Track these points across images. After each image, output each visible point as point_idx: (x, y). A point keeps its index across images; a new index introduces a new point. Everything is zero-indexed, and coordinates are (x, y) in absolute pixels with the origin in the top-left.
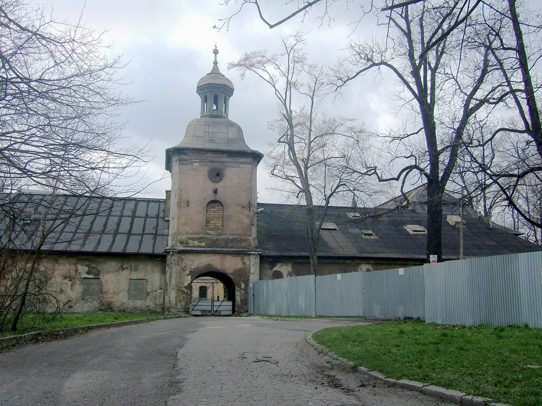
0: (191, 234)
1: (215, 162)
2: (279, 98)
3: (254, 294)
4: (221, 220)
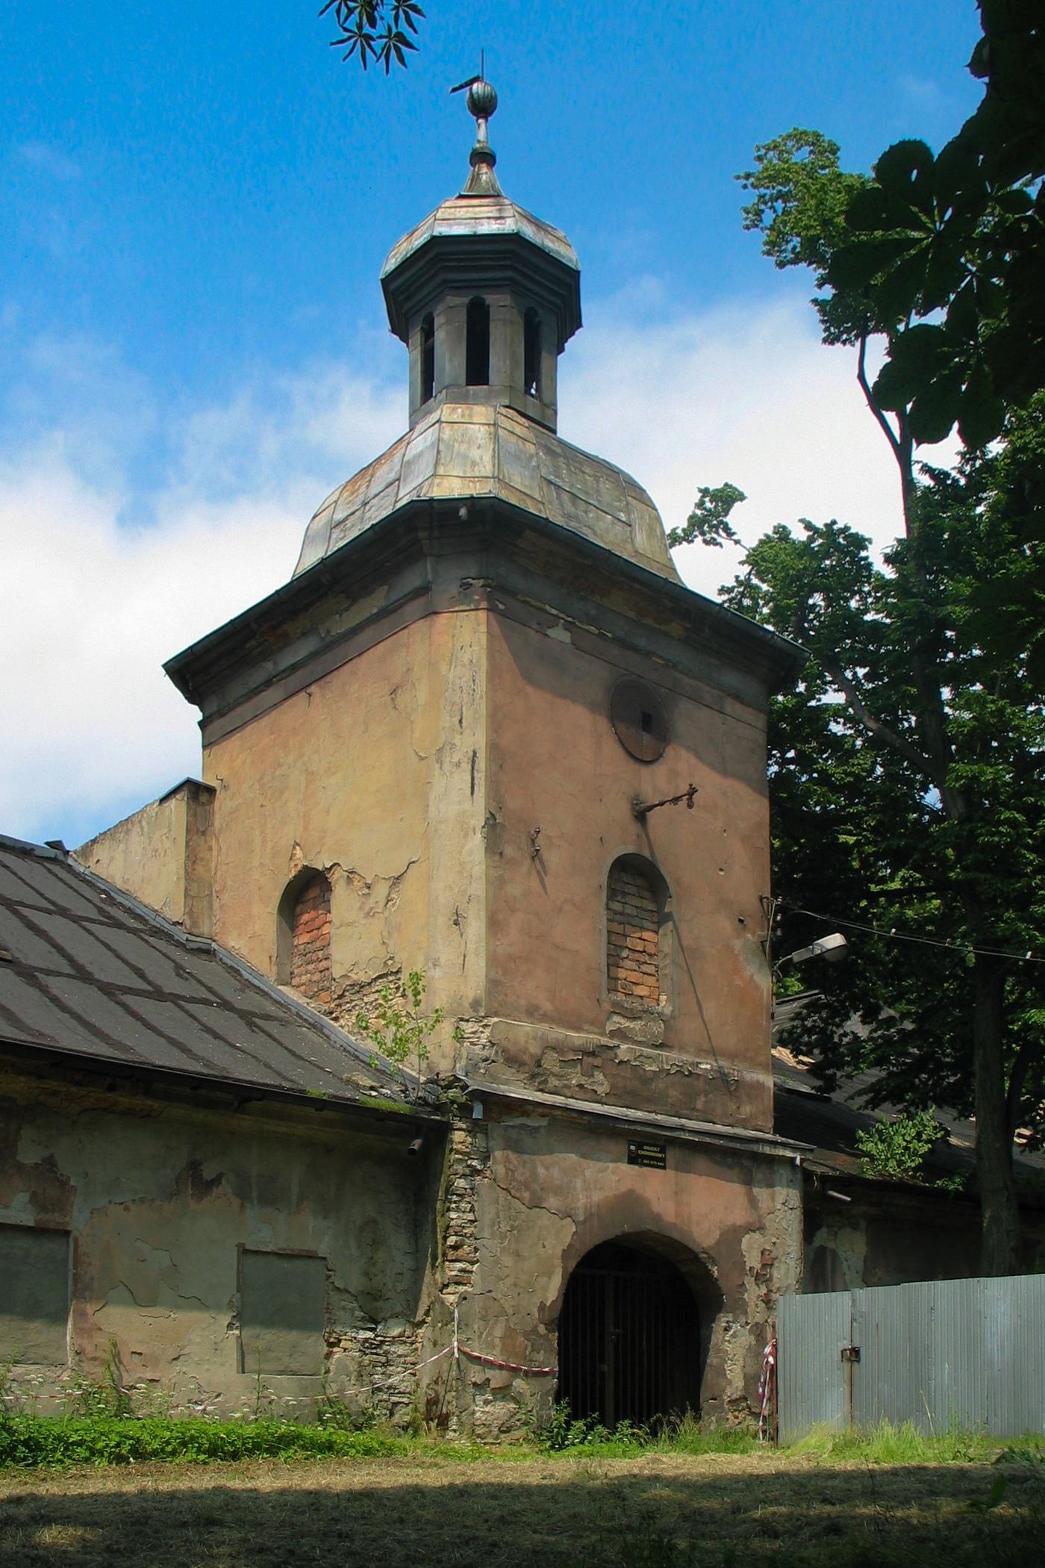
0: (545, 1018)
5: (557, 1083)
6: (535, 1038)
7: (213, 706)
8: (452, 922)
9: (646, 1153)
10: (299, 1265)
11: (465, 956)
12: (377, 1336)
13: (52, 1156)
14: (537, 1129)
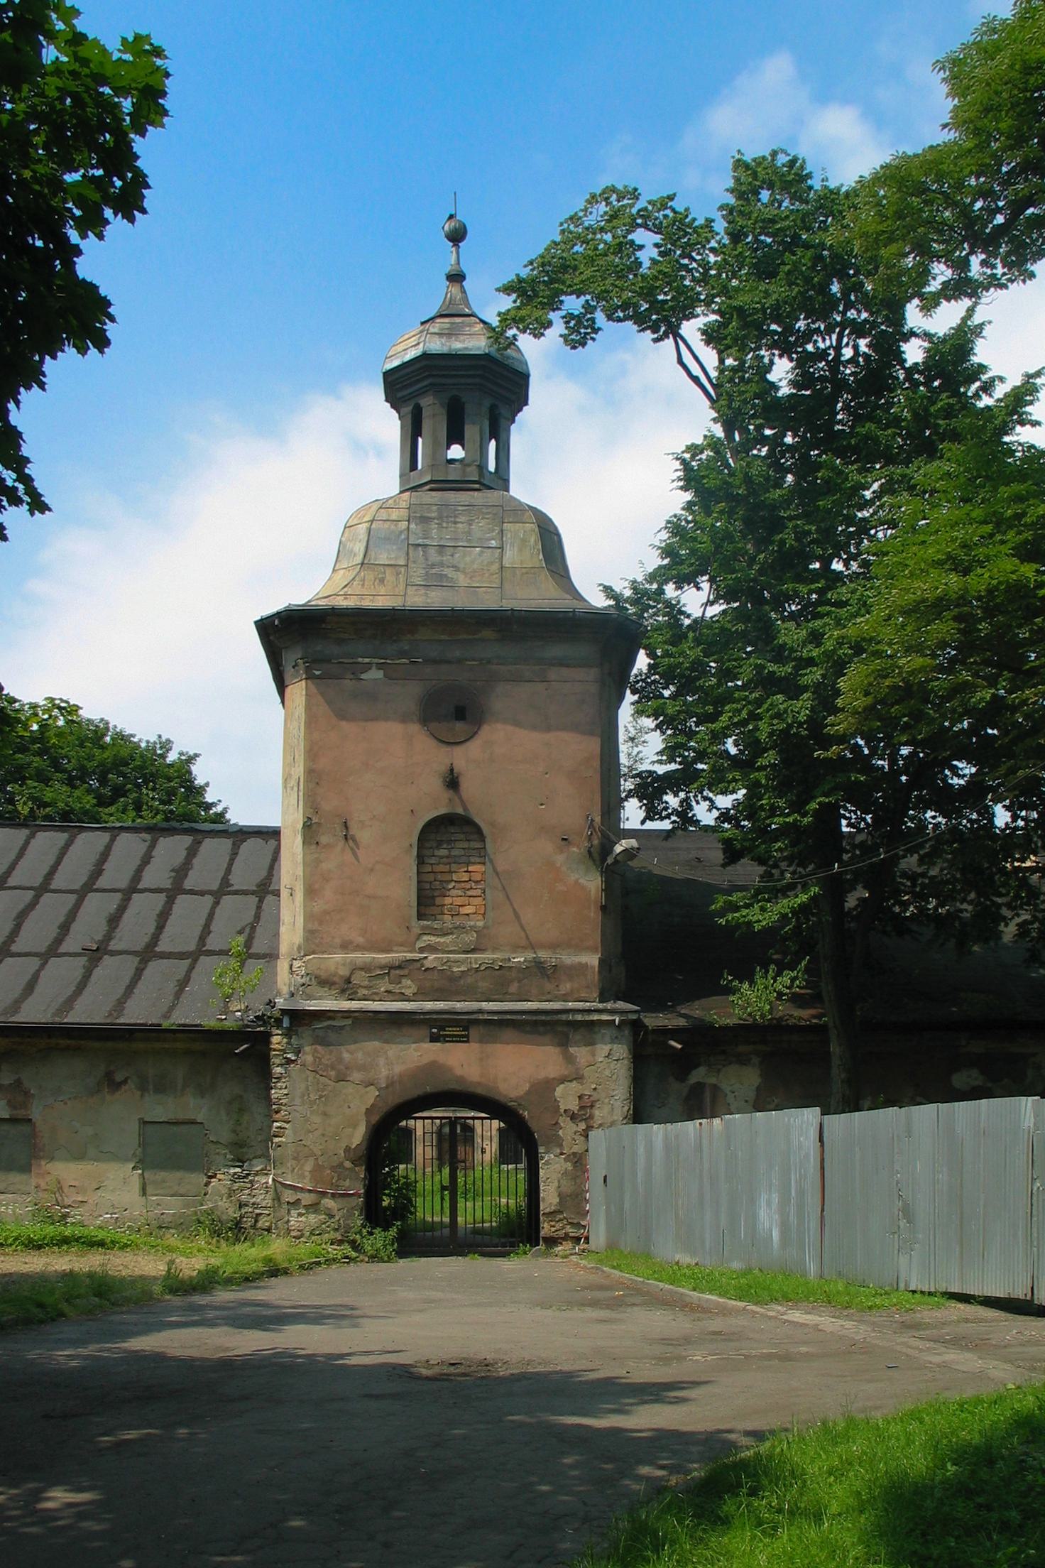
0: (358, 948)
1: (448, 662)
2: (696, 380)
3: (605, 1177)
4: (479, 892)
5: (366, 992)
6: (344, 965)
10: (184, 1128)
14: (342, 1028)
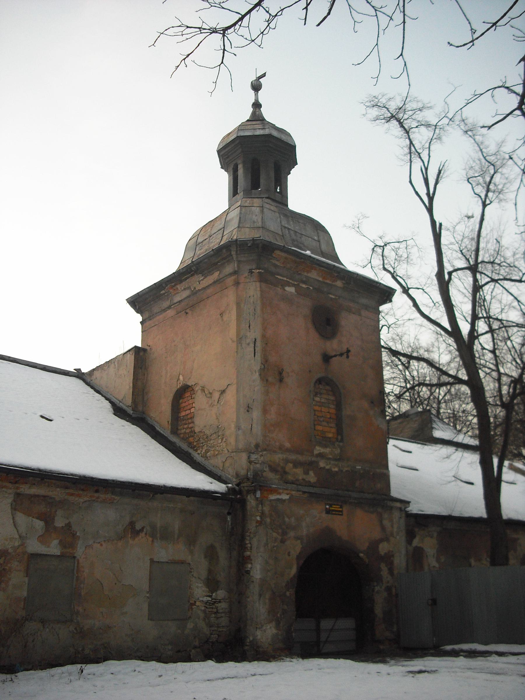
0: (288, 450)
7: (147, 315)
8: (246, 410)
9: (333, 509)
11: (252, 425)
12: (212, 599)
13: (69, 523)
